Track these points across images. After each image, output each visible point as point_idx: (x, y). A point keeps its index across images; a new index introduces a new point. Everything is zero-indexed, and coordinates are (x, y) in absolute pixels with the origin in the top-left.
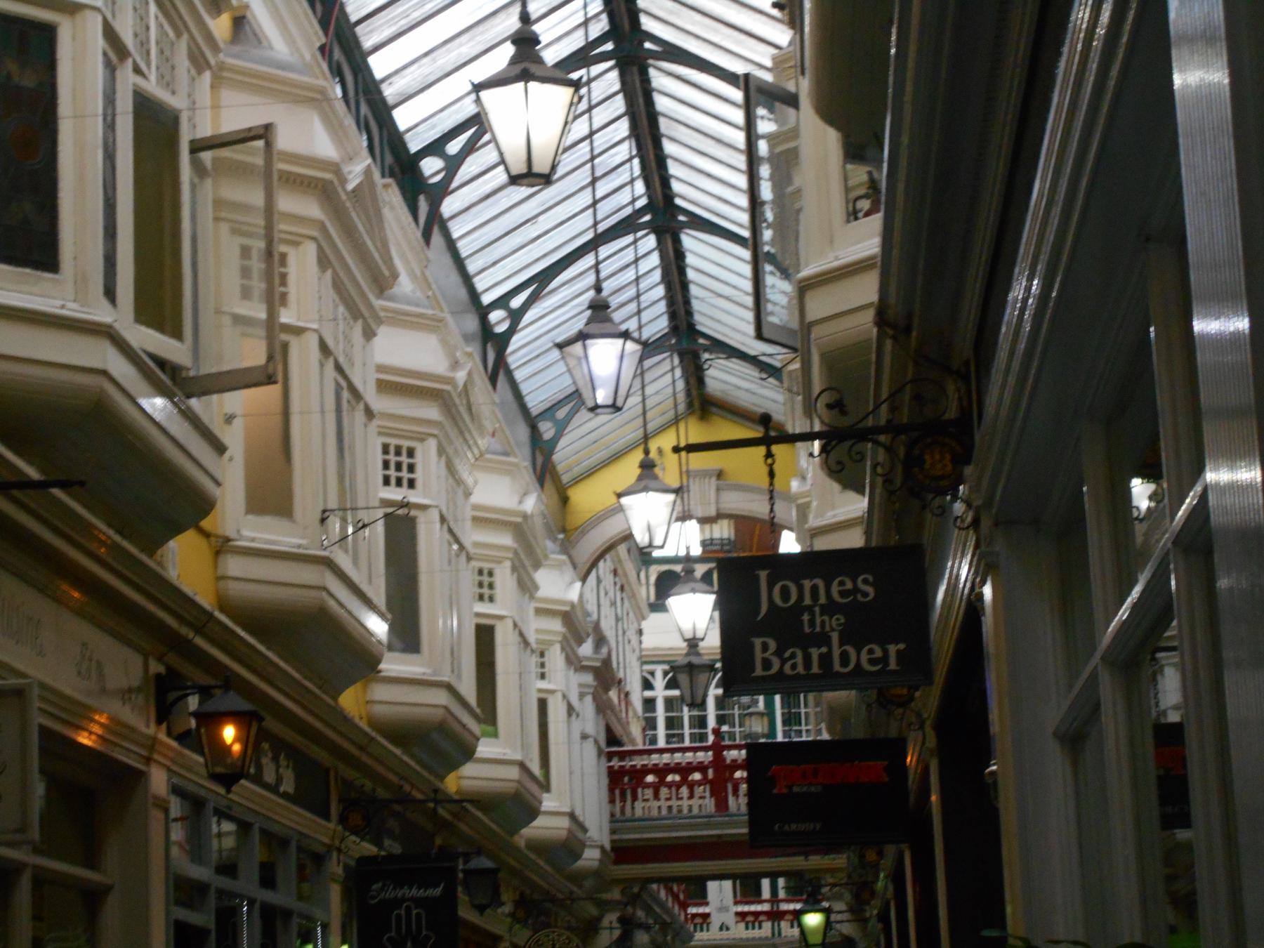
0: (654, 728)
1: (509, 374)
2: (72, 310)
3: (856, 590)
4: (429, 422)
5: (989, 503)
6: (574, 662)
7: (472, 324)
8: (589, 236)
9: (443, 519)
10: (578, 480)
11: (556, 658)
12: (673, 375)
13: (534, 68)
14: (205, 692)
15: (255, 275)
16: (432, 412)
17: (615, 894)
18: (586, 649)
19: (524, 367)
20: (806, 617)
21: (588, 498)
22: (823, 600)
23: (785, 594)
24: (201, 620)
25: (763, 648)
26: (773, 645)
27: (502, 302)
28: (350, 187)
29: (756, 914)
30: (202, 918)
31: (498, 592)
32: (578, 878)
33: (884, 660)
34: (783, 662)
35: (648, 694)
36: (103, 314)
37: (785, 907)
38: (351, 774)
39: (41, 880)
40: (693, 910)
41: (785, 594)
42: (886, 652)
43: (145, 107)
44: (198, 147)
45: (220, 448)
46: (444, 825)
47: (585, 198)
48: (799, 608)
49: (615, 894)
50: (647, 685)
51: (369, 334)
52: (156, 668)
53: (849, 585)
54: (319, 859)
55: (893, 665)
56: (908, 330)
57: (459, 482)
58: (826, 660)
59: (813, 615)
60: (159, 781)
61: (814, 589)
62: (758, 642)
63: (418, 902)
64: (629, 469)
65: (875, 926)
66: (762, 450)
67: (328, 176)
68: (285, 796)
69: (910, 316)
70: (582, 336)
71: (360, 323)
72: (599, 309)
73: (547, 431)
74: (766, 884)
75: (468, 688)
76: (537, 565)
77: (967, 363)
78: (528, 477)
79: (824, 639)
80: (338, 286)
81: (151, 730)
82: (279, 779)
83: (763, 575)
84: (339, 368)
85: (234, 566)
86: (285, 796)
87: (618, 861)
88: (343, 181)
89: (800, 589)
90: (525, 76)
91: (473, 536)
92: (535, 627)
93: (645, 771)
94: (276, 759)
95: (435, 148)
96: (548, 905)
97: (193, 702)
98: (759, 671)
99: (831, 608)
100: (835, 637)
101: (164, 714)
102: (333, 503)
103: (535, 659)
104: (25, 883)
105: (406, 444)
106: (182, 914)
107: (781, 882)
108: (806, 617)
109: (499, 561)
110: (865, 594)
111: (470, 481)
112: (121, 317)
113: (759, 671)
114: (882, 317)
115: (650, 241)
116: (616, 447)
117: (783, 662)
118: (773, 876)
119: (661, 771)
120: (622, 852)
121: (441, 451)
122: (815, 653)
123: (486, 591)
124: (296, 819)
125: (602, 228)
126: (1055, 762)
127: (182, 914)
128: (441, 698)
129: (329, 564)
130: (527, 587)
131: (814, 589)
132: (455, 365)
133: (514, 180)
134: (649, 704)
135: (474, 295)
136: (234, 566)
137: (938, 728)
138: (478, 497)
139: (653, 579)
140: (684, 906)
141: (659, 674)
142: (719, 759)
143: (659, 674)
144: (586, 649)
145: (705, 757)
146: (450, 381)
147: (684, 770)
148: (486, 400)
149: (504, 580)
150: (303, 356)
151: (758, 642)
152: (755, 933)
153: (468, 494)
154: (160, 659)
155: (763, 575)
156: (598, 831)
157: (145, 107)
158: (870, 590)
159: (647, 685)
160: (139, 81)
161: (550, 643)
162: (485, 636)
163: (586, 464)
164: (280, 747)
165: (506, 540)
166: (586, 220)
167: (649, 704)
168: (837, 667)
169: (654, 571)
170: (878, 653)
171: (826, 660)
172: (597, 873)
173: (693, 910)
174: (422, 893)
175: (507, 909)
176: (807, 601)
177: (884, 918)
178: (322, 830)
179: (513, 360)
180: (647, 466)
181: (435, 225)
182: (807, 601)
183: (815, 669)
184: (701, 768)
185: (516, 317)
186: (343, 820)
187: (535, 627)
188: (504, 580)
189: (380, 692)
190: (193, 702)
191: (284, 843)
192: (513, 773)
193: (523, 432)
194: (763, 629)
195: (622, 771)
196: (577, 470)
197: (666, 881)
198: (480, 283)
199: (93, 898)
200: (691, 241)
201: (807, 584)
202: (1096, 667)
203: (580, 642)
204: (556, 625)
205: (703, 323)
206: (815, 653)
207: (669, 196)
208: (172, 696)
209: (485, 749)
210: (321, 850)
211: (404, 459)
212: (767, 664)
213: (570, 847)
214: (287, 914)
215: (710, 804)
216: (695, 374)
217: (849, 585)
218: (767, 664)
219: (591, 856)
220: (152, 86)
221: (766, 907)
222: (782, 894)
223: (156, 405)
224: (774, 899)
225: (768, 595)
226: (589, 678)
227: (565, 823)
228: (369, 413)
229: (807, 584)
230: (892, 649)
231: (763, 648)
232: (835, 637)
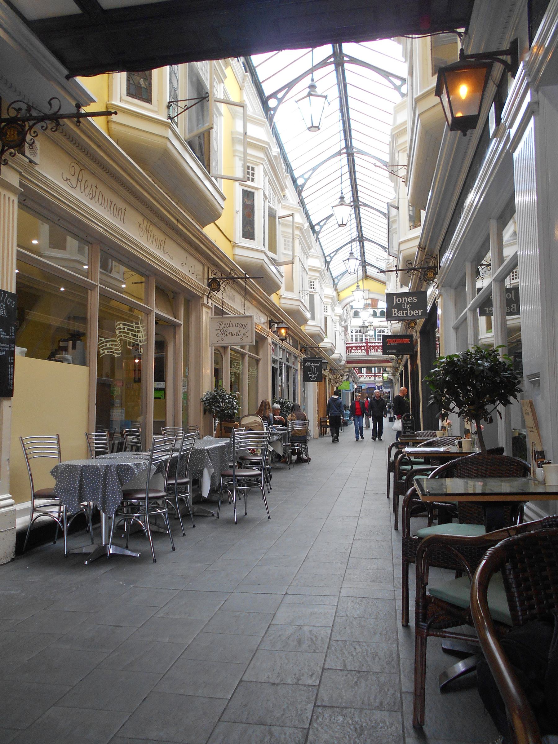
0: (356, 339)
1: (330, 269)
2: (257, 248)
3: (413, 300)
4: (317, 276)
5: (441, 282)
6: (341, 325)
7: (323, 259)
8: (350, 240)
9: (319, 295)
10: (341, 291)
11: (338, 324)
12: (60, 508)
13: (343, 203)
14: (278, 323)
15: (290, 242)
16: (317, 274)
17: (347, 370)
18: (343, 323)
19: (293, 301)
20: (403, 305)
21: (343, 295)
22: (406, 302)
23: (399, 300)
24: (278, 310)
25: (394, 311)
26: (396, 310)
27: (329, 255)
28: (305, 229)
29: (371, 376)
30: (277, 366)
31: (328, 310)
32: (340, 366)
33: (418, 313)
34: (398, 313)
35: (352, 334)
36: (263, 249)
37: (377, 375)
38: (302, 342)
39: (249, 356)
40: (359, 375)
41: (399, 300)
42: (419, 312)
43: (270, 208)
44: (280, 218)
45: (282, 277)
46: (318, 354)
47: (349, 233)
48: (402, 303)
49: (347, 370)
50: (352, 332)
51: (307, 258)
52: (269, 319)
53: (412, 299)
54: (296, 358)
55: (420, 314)
56: (425, 249)
57: (322, 288)
58: (407, 313)
59: (404, 304)
60: (270, 340)
61: (405, 299)
62: (393, 310)
63: (315, 366)
64: (355, 287)
65: (398, 376)
66: (395, 272)
67: (301, 226)
68: (291, 345)
69: (425, 246)
70: (348, 259)
71: (306, 256)
72: (351, 254)
73: (336, 281)
74: (373, 369)
75: (323, 328)
76: (335, 306)
77: (437, 255)
78: (333, 289)
79: (406, 309)
80: (302, 248)
81: (268, 330)
82: (290, 342)
83: (395, 297)
84: (302, 264)
85: (283, 301)
86: (291, 345)
87: (347, 364)
88: (304, 227)
89: (402, 299)
90: (342, 204)
91: (324, 300)
92: (335, 318)
93: (353, 347)
94: (289, 338)
95: (318, 224)
96: (335, 371)
97: (276, 325)
98: (393, 315)
99: (408, 303)
100: (409, 309)
101: (270, 327)
102: (301, 290)
103: (334, 324)
104: (247, 356)
105: (312, 280)
106: (273, 365)
107: (376, 368)
108: (403, 305)
109: (328, 305)
110: (415, 301)
111: (324, 289)
112: (266, 249)
113: (393, 315)
114: (419, 247)
115: (358, 243)
116: (349, 285)
117: (398, 313)
118: (375, 367)
119: (356, 347)
120: (349, 362)
121: (319, 282)
122: (404, 312)
123: (326, 310)
124: (293, 350)
125: (352, 239)
126: (452, 333)
127: (273, 365)
128: (319, 329)
129: (300, 301)
130: (333, 310)
131: (405, 299)
132: (322, 265)
133: (340, 225)
134: (352, 336)
135: (324, 254)
136: (283, 301)
137: (420, 332)
138: (325, 292)
139: (353, 312)
140: (358, 374)
141: (354, 330)
142: (367, 346)
143: (354, 330)
144: (343, 323)
145: (364, 344)
146: (321, 268)
147: (360, 347)
148: (327, 274)
149: (329, 308)
150: (297, 260)
151: (393, 310)
152: (371, 379)
153: (323, 291)
154: (270, 317)
155: (395, 297)
156: (344, 358)
157: (270, 208)
158: (416, 300)
159: (352, 332)
160: (269, 204)
161: (337, 321)
162: (326, 318)
163: (343, 288)
164: (290, 336)
165: (330, 300)
166: (350, 237)
167: (352, 336)
168: (409, 315)
169: (353, 311)
170: (417, 312)
171: (407, 313)
172: (344, 366)
173: (359, 375)
174: (315, 365)
175: (328, 371)
176: (403, 302)
177: (401, 375)
178: (297, 352)
179: (330, 267)
180: (358, 286)
181: (317, 239)
182: (403, 302)
183: (405, 315)
184: (364, 347)
185: (332, 258)
186: (301, 351)
187: (335, 318)
188: (329, 308)
189: (307, 327)
190: (276, 325)
191: (290, 354)
192: (331, 345)
193: (332, 281)
194: (394, 307)
195: (349, 347)
196: (341, 289)
197: (354, 368)
198: (325, 252)
199: (258, 361)
200: (366, 243)
201: (403, 298)
202: (467, 311)
203: (342, 321)
204: (338, 318)
205: (367, 260)
206: (404, 312)
207: (362, 235)
208: (272, 324)
209: (326, 340)
210: (297, 356)
211: (312, 283)
212: (395, 314)
213: (340, 360)
214: (291, 367)
215: (365, 354)
216: (365, 271)
217: (412, 299)
218: (395, 314)
219: (343, 362)
220: (271, 205)
221: (373, 375)
222: (376, 372)
223: (272, 268)
224: (375, 373)
225: (396, 300)
226: (343, 329)
227: (339, 355)
228: (307, 273)
229: (403, 298)
230: (420, 311)
231: (394, 311)
232: (409, 309)
